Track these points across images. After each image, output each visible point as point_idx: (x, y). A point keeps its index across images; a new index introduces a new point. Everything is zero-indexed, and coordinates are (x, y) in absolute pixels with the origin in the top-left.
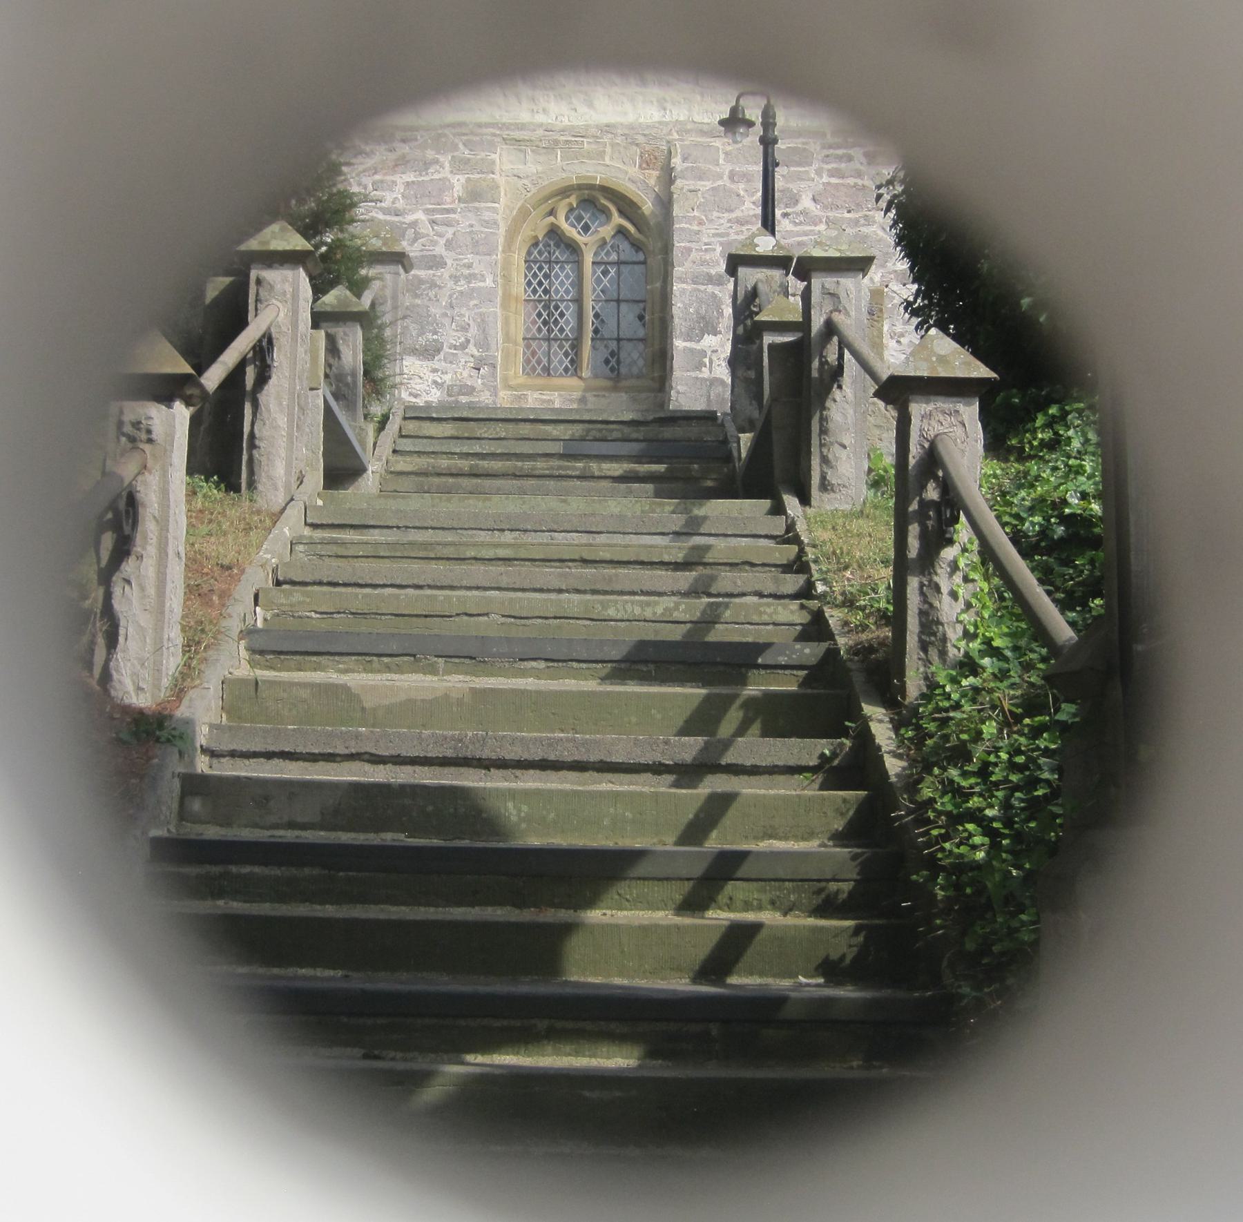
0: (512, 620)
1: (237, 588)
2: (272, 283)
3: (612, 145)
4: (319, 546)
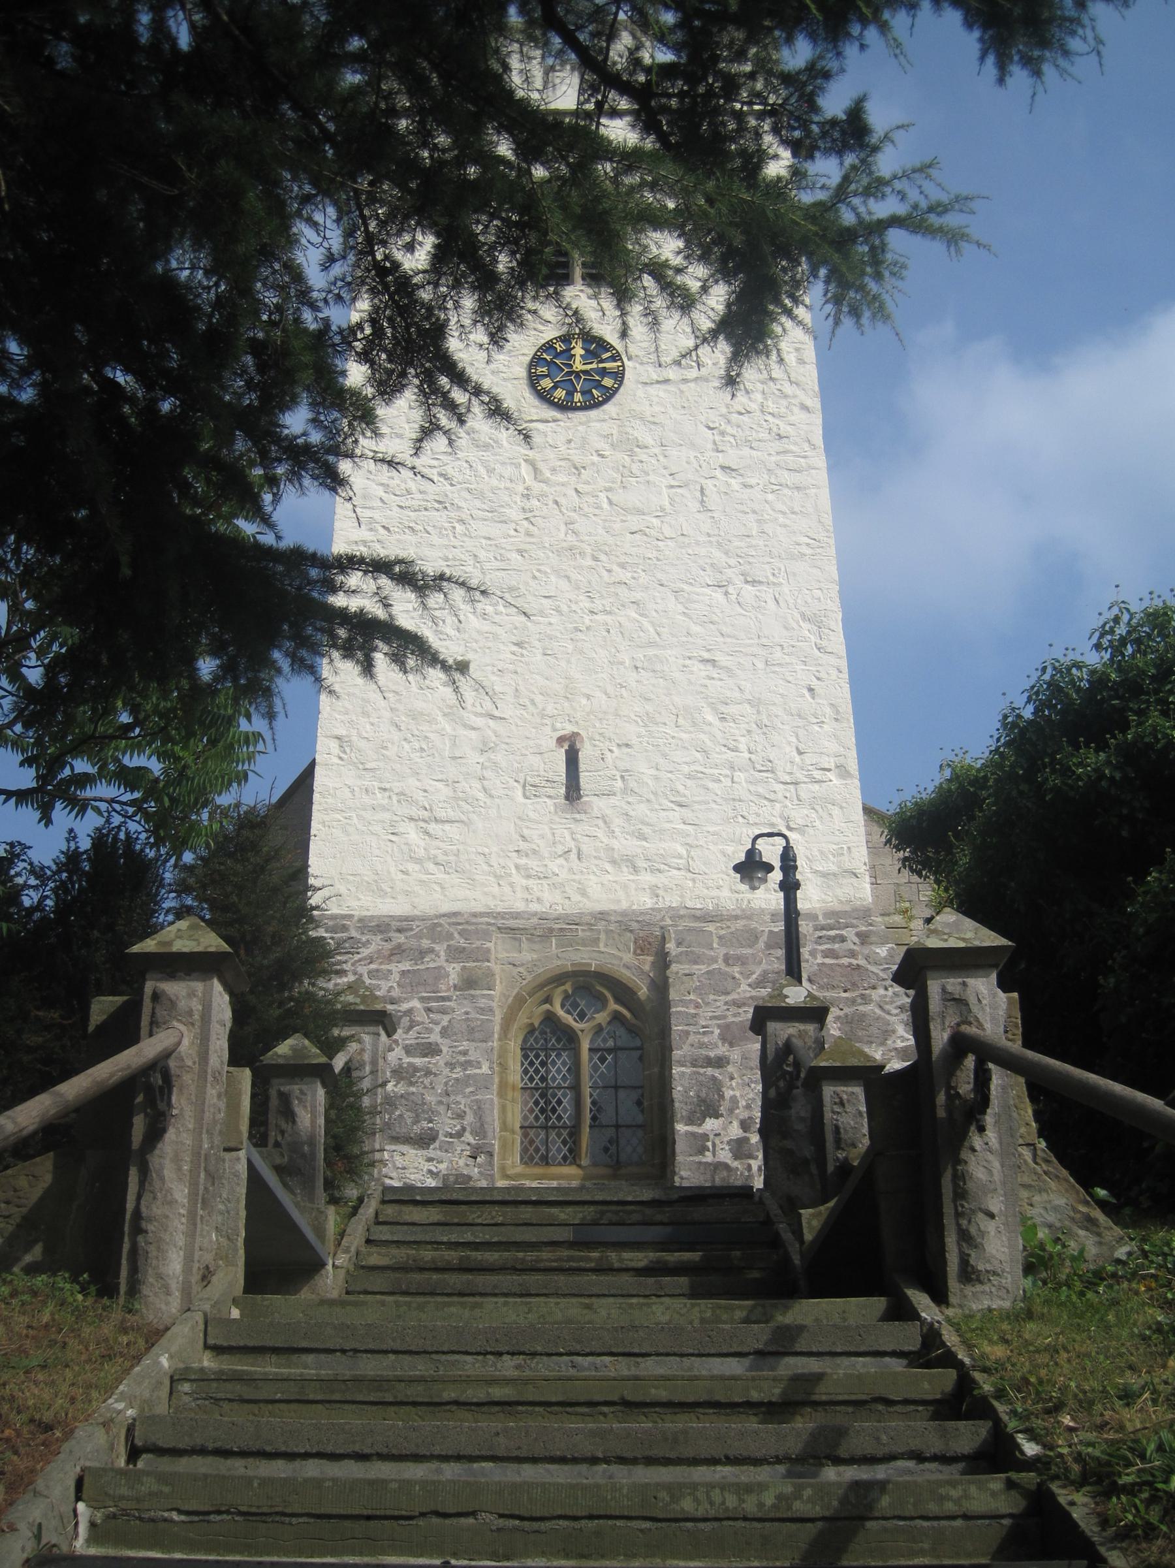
0: (517, 1522)
1: (48, 1468)
2: (174, 998)
4: (214, 1385)
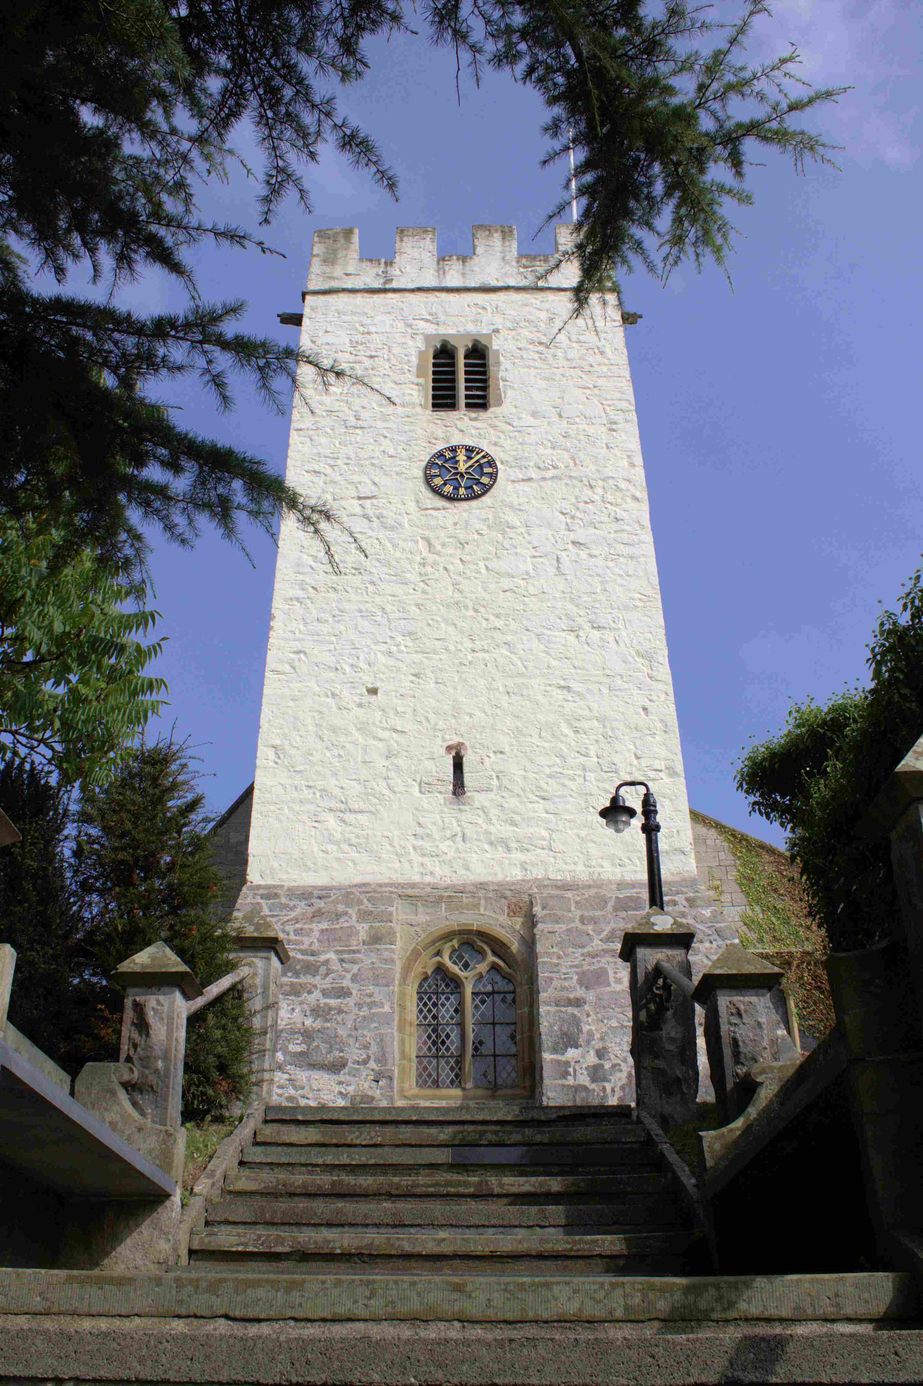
3: (486, 899)
